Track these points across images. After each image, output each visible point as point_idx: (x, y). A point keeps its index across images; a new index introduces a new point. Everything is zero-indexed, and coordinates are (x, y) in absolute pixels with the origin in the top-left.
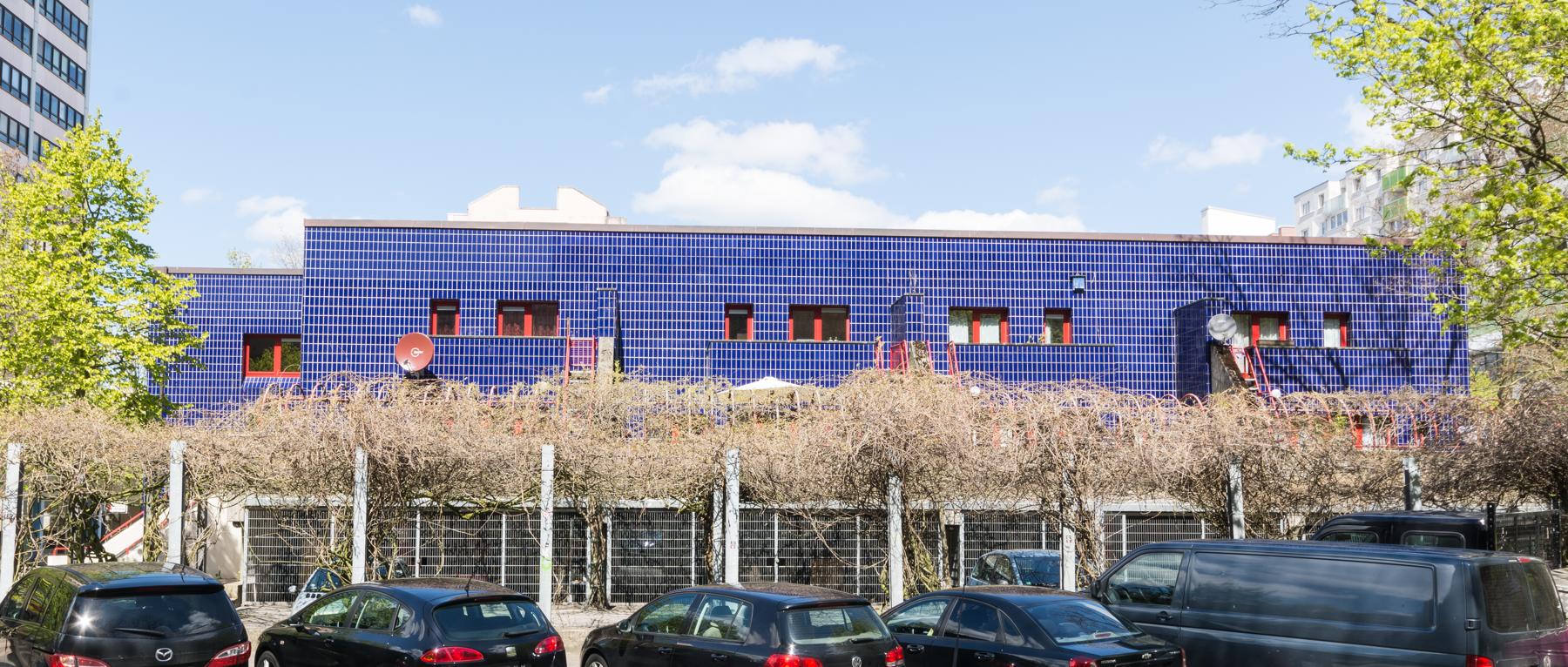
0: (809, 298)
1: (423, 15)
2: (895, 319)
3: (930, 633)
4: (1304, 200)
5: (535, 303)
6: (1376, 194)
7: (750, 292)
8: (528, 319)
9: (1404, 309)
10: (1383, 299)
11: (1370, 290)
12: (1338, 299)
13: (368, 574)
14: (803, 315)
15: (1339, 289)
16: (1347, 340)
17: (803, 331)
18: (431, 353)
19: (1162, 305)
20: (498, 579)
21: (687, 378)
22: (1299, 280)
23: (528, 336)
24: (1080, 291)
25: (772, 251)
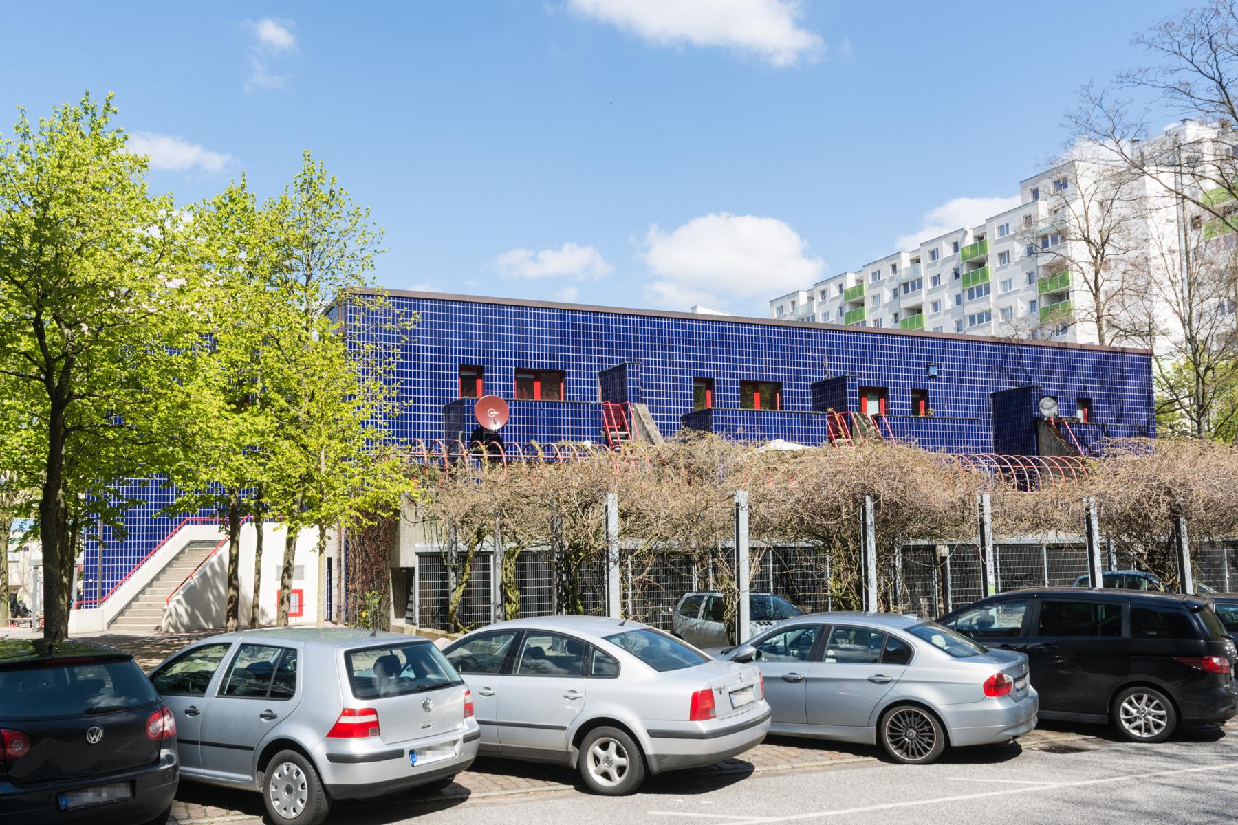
0: (754, 375)
1: (273, 33)
2: (1122, 409)
3: (65, 580)
4: (778, 304)
5: (543, 371)
6: (838, 303)
7: (712, 368)
8: (537, 385)
9: (1120, 397)
10: (1110, 389)
11: (1102, 383)
12: (1085, 388)
13: (997, 591)
14: (749, 386)
15: (1084, 382)
16: (1088, 416)
17: (746, 400)
18: (507, 418)
19: (983, 387)
20: (1044, 583)
21: (943, 448)
22: (1063, 374)
23: (537, 398)
24: (934, 377)
25: (726, 335)
